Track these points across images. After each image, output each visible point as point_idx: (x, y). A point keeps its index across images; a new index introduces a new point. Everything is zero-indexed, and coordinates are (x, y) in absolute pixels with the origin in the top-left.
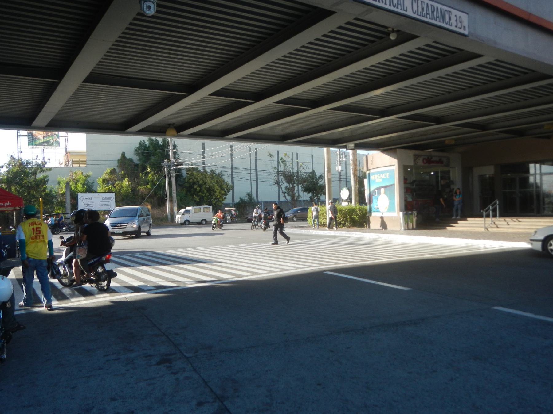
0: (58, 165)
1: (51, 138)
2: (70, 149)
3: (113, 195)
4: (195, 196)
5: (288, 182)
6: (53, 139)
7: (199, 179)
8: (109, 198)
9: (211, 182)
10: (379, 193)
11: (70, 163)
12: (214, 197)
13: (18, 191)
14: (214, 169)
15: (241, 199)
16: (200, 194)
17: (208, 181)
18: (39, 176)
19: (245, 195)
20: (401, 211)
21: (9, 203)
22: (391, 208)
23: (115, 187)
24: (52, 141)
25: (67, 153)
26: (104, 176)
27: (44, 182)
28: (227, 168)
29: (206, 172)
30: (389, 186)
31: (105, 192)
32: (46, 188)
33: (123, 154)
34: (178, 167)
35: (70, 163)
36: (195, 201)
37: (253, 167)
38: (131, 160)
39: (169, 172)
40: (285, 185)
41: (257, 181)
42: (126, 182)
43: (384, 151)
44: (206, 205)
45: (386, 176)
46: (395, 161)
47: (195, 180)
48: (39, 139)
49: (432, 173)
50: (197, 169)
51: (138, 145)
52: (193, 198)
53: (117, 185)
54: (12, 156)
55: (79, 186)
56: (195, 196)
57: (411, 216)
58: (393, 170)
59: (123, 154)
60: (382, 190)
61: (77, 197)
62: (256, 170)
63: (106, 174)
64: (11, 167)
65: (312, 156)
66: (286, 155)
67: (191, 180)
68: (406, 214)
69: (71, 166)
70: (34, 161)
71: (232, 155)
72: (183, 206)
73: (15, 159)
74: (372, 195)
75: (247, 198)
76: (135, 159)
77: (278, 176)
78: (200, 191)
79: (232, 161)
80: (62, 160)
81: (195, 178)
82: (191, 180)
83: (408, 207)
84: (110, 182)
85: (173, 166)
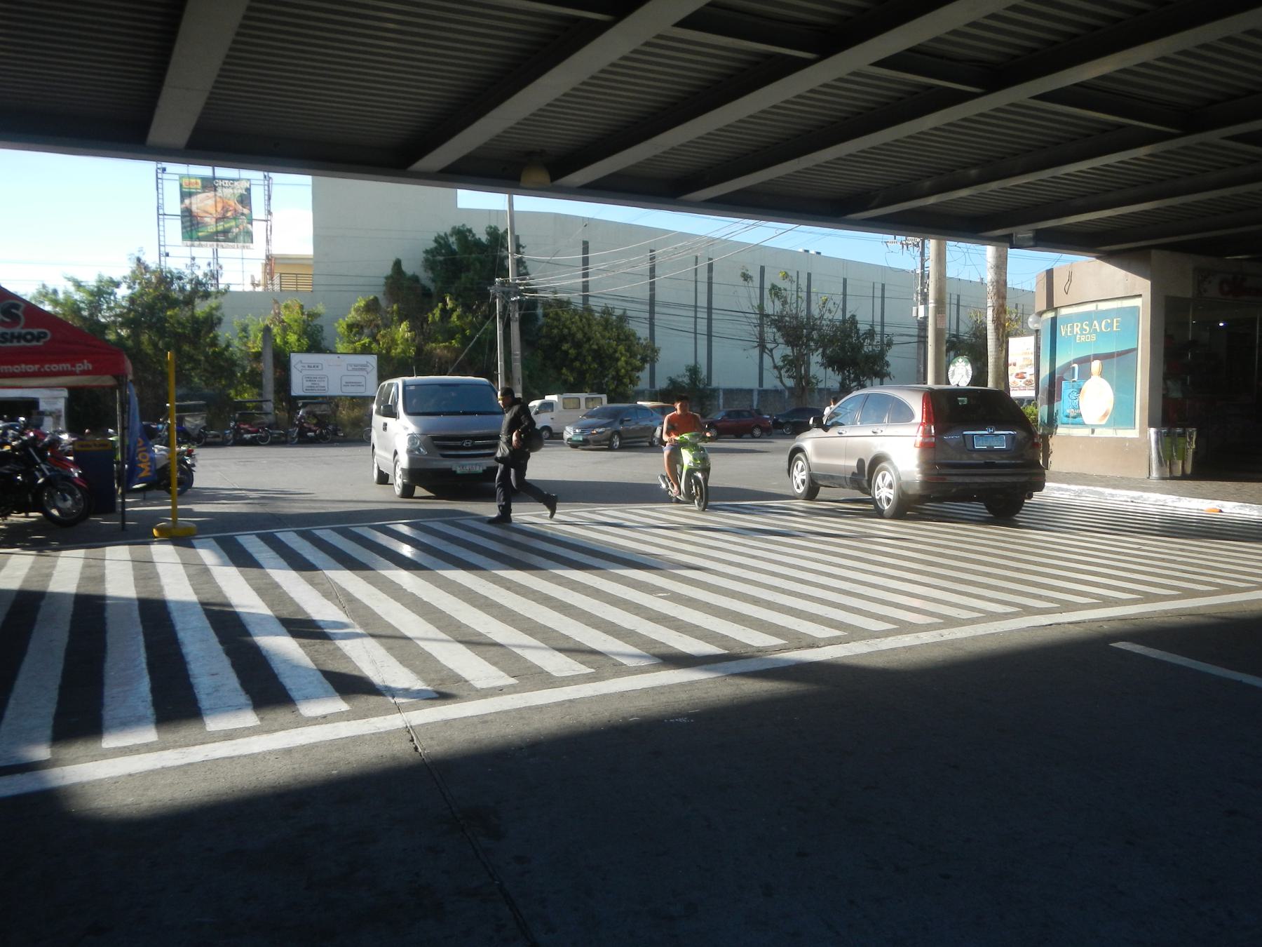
0: (249, 288)
1: (233, 223)
2: (277, 250)
3: (372, 360)
4: (564, 371)
5: (788, 343)
6: (237, 226)
7: (574, 329)
8: (363, 368)
9: (603, 337)
10: (1086, 375)
11: (277, 280)
12: (612, 373)
13: (155, 345)
14: (610, 303)
15: (672, 381)
16: (577, 364)
17: (597, 332)
18: (201, 308)
19: (683, 370)
20: (1151, 424)
21: (87, 365)
22: (1120, 415)
23: (377, 342)
24: (235, 230)
25: (270, 259)
26: (352, 316)
27: (211, 322)
28: (641, 303)
29: (590, 311)
30: (1120, 354)
31: (355, 352)
32: (215, 337)
33: (398, 264)
34: (528, 296)
35: (277, 280)
36: (565, 382)
37: (703, 301)
38: (415, 279)
39: (505, 307)
40: (782, 350)
41: (710, 335)
42: (403, 330)
43: (1109, 257)
44: (592, 391)
45: (1110, 325)
46: (1143, 285)
47: (566, 331)
48: (206, 225)
49: (22, 419)
50: (569, 303)
51: (433, 245)
52: (560, 374)
53: (383, 336)
54: (139, 260)
55: (292, 338)
56: (564, 371)
57: (1181, 440)
58: (1136, 308)
59: (398, 264)
60: (1096, 365)
61: (289, 361)
62: (710, 308)
63: (357, 310)
64: (137, 286)
65: (845, 280)
66: (786, 276)
67: (555, 331)
68: (1168, 434)
69: (277, 288)
70: (187, 272)
71: (652, 270)
72: (536, 392)
73: (146, 268)
74: (1062, 379)
75: (686, 380)
76: (425, 277)
77: (761, 325)
78: (576, 359)
79: (652, 284)
80: (259, 277)
81: (564, 326)
82: (555, 331)
83: (1169, 415)
84: (366, 331)
85: (519, 293)
